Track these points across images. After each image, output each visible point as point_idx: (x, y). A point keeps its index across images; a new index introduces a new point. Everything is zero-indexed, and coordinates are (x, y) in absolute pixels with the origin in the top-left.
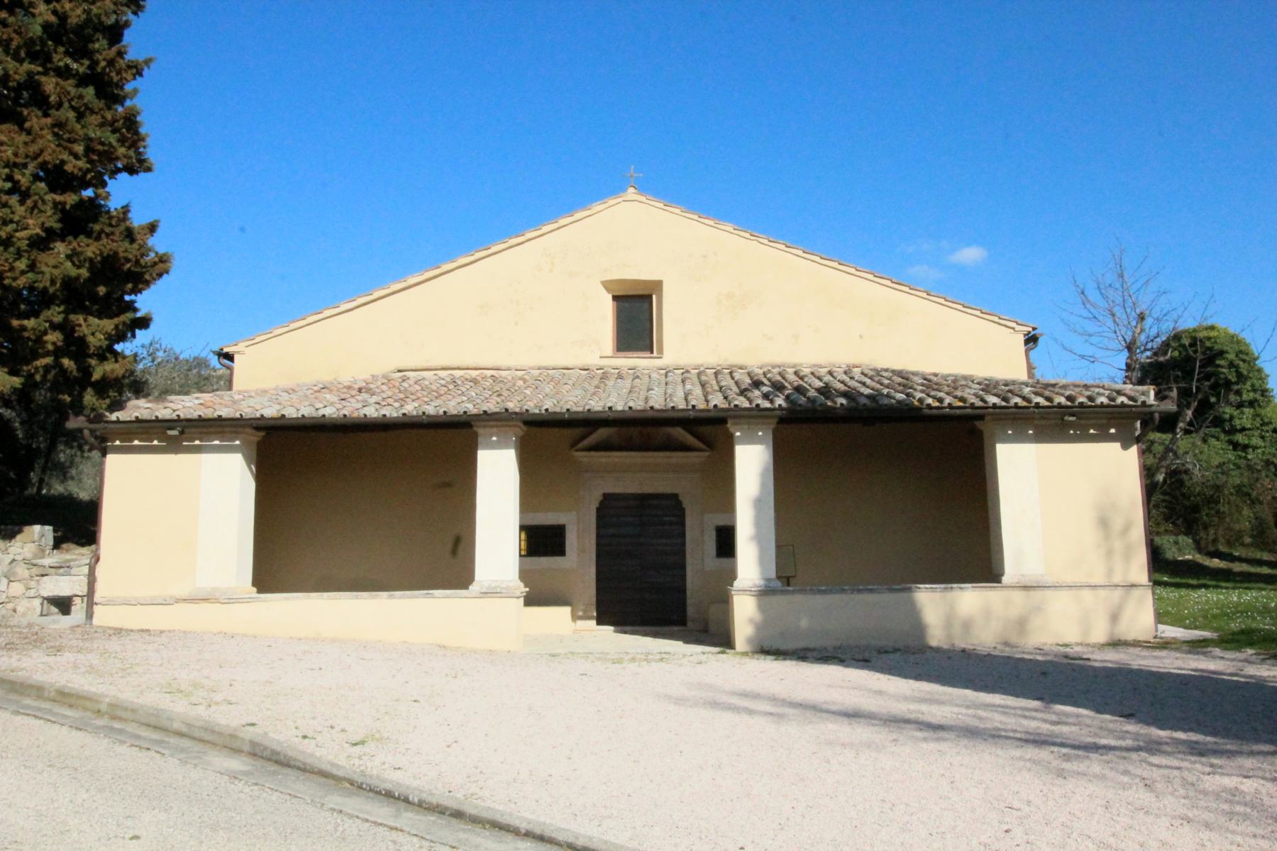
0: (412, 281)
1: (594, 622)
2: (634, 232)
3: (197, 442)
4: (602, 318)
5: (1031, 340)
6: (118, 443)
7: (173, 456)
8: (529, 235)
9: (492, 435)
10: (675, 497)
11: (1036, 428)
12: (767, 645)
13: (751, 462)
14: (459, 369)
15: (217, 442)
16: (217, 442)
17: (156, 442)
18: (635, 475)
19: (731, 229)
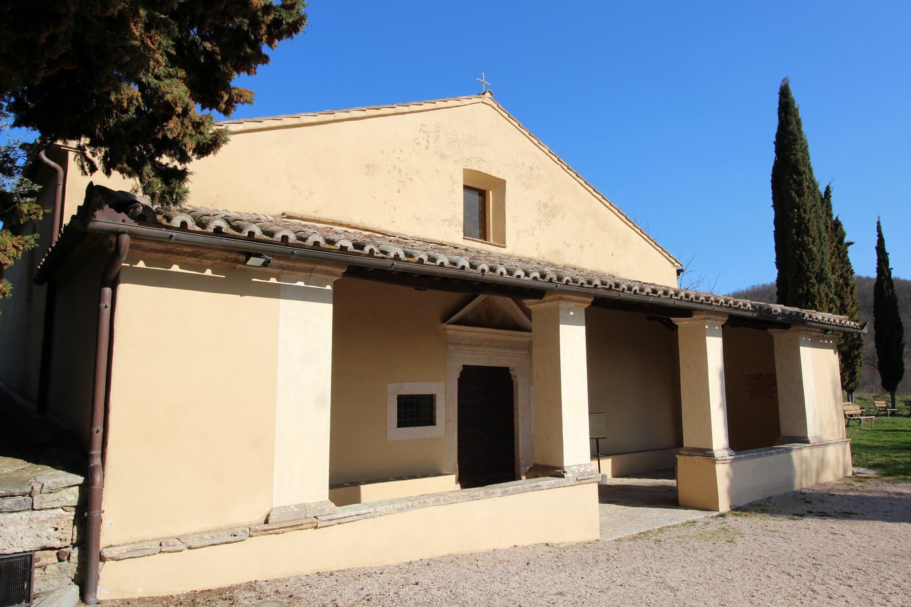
0: (305, 119)
1: (449, 482)
2: (478, 132)
3: (273, 280)
4: (454, 205)
5: (679, 272)
6: (141, 264)
7: (236, 298)
8: (384, 111)
9: (569, 310)
10: (506, 370)
11: (812, 337)
12: (742, 503)
13: (573, 341)
14: (341, 225)
15: (301, 284)
16: (301, 284)
17: (208, 272)
18: (483, 348)
19: (547, 151)
